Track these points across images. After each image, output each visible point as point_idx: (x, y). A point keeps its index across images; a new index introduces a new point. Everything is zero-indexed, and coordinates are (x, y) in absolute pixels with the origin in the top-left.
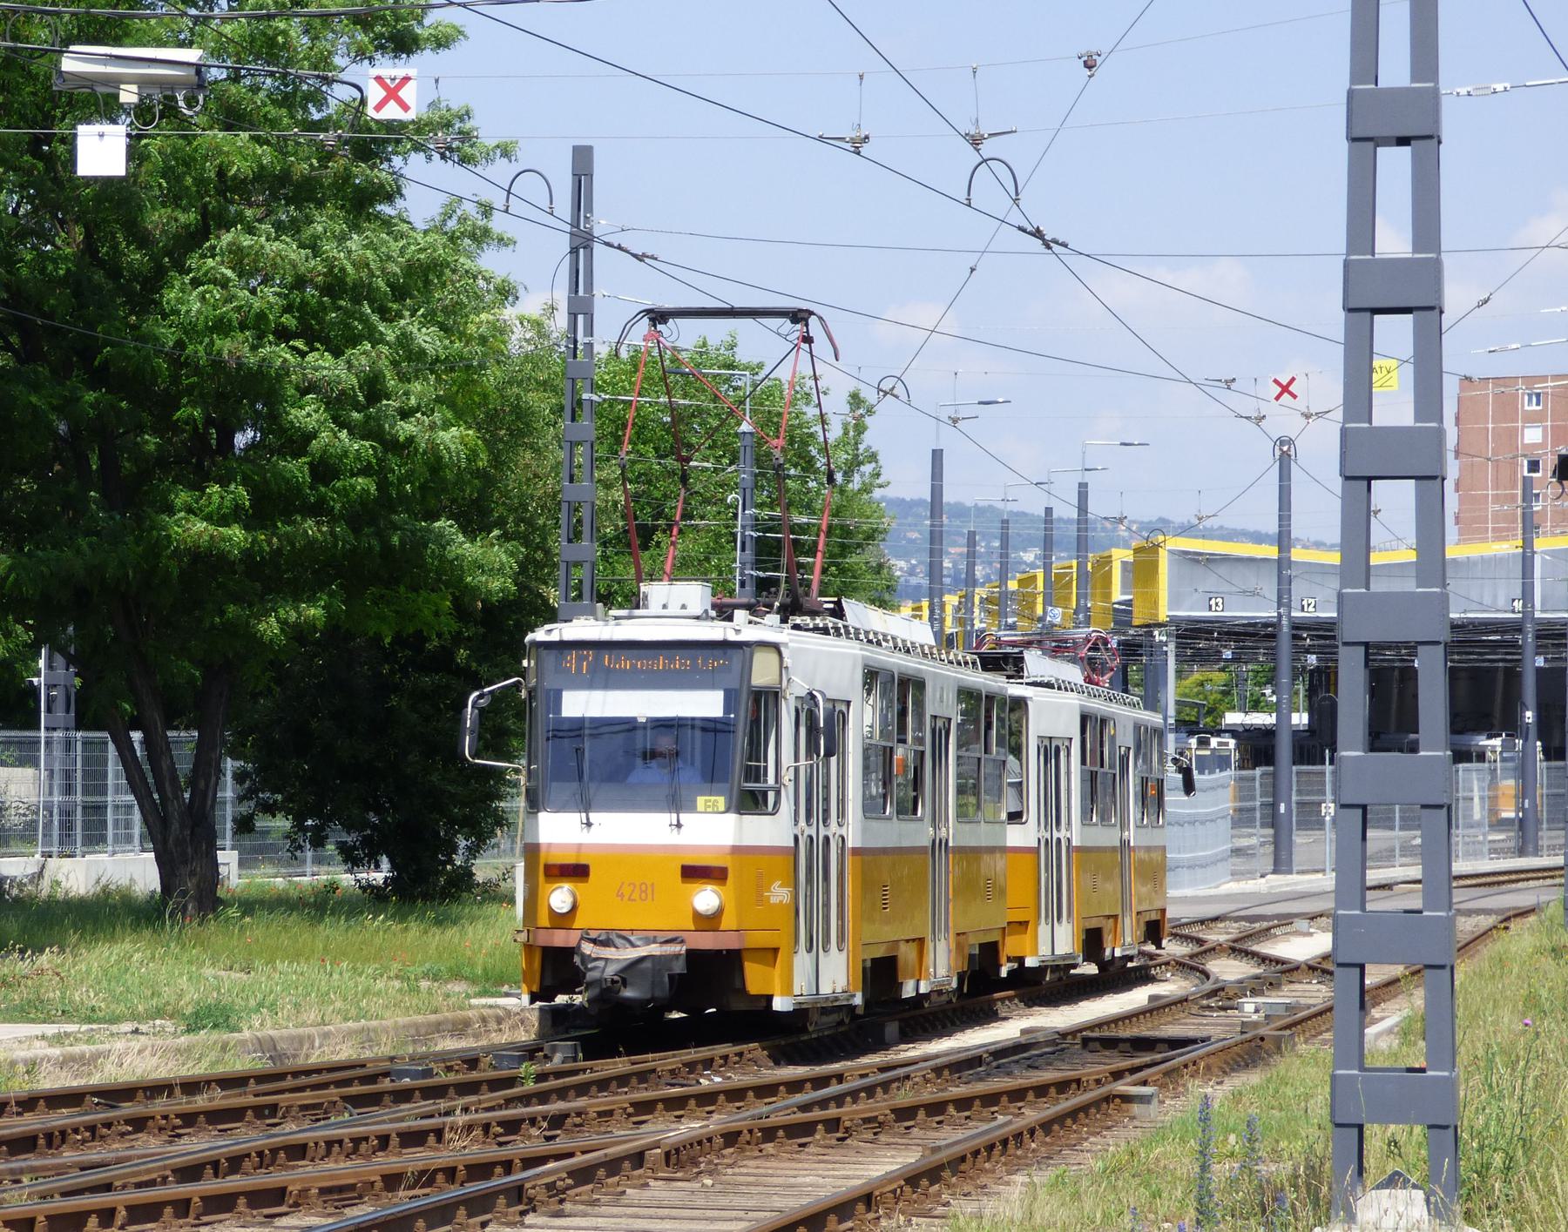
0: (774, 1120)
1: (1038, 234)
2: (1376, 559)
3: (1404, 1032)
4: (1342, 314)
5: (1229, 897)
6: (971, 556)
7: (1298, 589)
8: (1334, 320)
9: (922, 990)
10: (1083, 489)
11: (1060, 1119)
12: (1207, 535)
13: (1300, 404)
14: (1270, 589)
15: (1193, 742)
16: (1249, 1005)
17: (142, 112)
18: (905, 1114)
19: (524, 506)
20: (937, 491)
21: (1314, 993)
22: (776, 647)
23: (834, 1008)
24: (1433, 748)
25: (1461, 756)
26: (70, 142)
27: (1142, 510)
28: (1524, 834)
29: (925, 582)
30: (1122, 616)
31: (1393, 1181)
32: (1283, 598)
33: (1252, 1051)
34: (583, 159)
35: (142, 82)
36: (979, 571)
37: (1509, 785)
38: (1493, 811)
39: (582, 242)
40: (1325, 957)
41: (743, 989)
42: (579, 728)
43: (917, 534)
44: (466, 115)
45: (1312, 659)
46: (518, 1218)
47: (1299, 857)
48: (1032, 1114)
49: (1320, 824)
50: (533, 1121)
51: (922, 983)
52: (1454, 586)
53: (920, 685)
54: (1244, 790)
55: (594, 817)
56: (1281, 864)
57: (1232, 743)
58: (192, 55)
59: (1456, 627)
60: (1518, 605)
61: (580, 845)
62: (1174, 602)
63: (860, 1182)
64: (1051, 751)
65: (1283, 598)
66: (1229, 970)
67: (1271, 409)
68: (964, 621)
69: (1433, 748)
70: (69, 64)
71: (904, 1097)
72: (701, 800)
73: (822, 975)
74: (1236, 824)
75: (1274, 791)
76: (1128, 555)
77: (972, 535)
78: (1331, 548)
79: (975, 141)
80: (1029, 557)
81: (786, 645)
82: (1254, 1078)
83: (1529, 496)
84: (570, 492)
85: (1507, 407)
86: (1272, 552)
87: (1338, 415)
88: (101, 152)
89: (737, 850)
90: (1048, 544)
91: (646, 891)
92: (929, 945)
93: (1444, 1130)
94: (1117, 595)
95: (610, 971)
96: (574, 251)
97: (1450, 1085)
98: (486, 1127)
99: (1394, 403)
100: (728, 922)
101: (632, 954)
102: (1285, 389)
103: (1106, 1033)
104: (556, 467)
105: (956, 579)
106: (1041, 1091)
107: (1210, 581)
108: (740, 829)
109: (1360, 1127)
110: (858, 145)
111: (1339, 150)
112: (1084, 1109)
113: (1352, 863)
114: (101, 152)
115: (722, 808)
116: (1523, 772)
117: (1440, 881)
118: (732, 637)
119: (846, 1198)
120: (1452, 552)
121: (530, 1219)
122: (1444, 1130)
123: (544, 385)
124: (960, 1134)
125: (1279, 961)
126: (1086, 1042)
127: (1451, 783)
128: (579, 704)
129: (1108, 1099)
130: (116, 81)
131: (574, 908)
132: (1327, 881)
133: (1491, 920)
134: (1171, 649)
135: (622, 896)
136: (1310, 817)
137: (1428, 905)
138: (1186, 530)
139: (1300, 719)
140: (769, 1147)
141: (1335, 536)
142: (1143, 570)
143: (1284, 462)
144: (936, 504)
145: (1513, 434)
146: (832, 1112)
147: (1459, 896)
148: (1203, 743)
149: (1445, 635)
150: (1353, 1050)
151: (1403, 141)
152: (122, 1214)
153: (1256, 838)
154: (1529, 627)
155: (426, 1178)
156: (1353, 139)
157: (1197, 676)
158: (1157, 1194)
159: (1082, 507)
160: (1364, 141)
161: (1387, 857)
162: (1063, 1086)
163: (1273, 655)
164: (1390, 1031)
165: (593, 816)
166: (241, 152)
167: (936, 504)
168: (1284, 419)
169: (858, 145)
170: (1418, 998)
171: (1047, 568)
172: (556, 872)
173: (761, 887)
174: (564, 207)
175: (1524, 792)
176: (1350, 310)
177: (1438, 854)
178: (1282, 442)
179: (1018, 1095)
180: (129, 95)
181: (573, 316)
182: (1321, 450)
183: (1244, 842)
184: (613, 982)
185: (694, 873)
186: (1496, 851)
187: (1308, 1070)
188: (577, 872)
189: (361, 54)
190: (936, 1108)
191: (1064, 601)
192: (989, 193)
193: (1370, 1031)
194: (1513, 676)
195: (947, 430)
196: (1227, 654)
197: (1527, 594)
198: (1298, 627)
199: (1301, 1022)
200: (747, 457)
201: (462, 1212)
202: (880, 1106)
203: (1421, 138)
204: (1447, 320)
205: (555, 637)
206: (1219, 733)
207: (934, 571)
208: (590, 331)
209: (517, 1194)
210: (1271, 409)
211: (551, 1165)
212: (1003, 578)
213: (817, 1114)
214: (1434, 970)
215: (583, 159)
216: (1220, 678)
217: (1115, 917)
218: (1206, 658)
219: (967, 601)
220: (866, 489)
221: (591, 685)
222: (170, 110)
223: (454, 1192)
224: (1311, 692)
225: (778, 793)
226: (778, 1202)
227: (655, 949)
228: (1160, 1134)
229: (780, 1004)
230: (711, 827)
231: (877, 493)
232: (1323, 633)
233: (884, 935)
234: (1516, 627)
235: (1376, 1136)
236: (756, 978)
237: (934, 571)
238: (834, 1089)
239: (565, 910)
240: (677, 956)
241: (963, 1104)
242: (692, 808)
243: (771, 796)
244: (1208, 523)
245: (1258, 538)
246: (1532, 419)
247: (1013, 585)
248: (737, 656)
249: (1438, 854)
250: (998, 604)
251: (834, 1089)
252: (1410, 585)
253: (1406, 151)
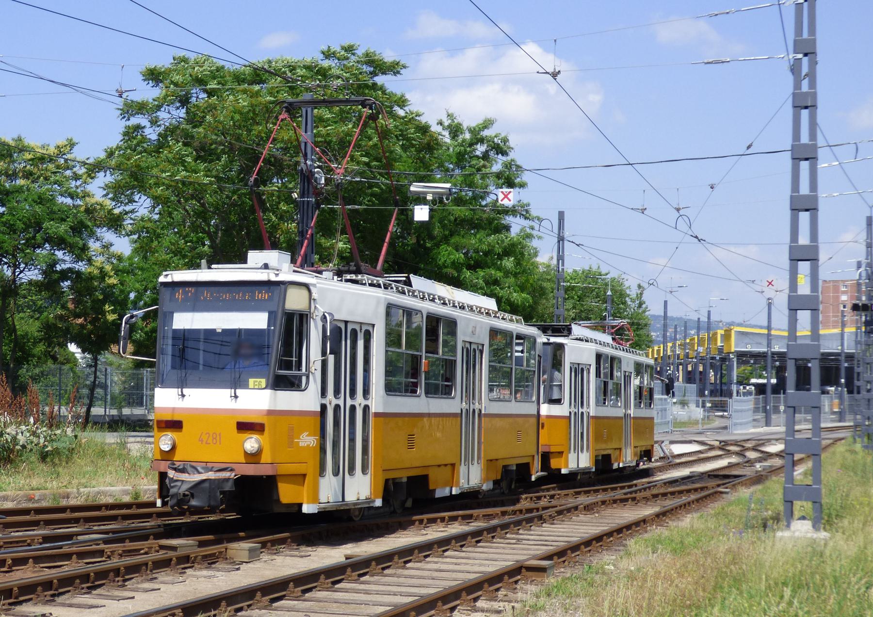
0: (616, 497)
1: (696, 237)
2: (798, 334)
3: (805, 474)
4: (788, 261)
5: (752, 434)
6: (676, 332)
7: (773, 342)
8: (786, 263)
9: (454, 493)
10: (709, 312)
11: (701, 498)
12: (746, 326)
13: (774, 288)
14: (765, 343)
15: (742, 387)
16: (758, 466)
17: (434, 202)
18: (655, 496)
19: (543, 316)
20: (665, 312)
21: (777, 462)
22: (306, 286)
23: (585, 472)
24: (815, 391)
25: (824, 392)
26: (412, 211)
27: (727, 319)
28: (841, 416)
29: (662, 340)
30: (720, 351)
31: (803, 518)
32: (769, 345)
33: (759, 479)
34: (561, 215)
35: (433, 193)
36: (678, 336)
37: (836, 401)
38: (831, 409)
39: (561, 239)
40: (781, 452)
41: (278, 500)
42: (185, 338)
43: (659, 325)
44: (529, 205)
45: (778, 363)
46: (380, 571)
47: (773, 422)
48: (693, 497)
49: (779, 412)
50: (545, 497)
51: (454, 489)
52: (821, 342)
53: (452, 325)
54: (757, 402)
55: (186, 391)
56: (768, 424)
57: (753, 388)
58: (448, 185)
59: (823, 354)
60: (840, 348)
61: (174, 409)
62: (736, 346)
63: (411, 599)
64: (578, 370)
65: (769, 345)
66: (752, 455)
67: (766, 289)
68: (673, 351)
69: (815, 391)
70: (412, 189)
71: (655, 491)
72: (251, 381)
73: (581, 460)
74: (754, 412)
75: (766, 402)
76: (723, 332)
77: (676, 326)
78: (784, 330)
79: (678, 210)
80: (693, 332)
81: (314, 285)
82: (759, 487)
83: (843, 316)
84: (557, 312)
85: (836, 289)
86: (765, 331)
87: (787, 291)
88: (421, 214)
89: (270, 413)
90: (699, 329)
91: (216, 438)
92: (624, 450)
93: (817, 503)
94: (719, 344)
95: (185, 487)
96: (559, 242)
97: (819, 490)
98: (531, 498)
99: (804, 287)
100: (266, 457)
101: (197, 478)
102: (770, 283)
103: (715, 473)
104: (553, 306)
105: (671, 338)
106: (696, 490)
107: (747, 340)
108: (274, 400)
109: (792, 502)
110: (643, 211)
111: (788, 213)
112: (709, 495)
113: (791, 424)
114: (421, 214)
115: (264, 386)
116: (841, 397)
117: (817, 430)
118: (273, 278)
119: (498, 573)
120: (822, 332)
121: (544, 525)
122: (817, 503)
123: (549, 280)
124: (671, 502)
125: (767, 453)
126: (709, 476)
127: (820, 399)
128: (183, 321)
129: (716, 493)
130: (426, 193)
131: (174, 448)
132: (783, 429)
133: (831, 441)
134: (735, 359)
135: (202, 441)
136: (776, 410)
137: (814, 437)
138: (739, 325)
139: (774, 381)
140: (615, 505)
141: (786, 327)
142: (727, 337)
143: (770, 305)
144: (665, 316)
145: (838, 297)
146: (634, 495)
147: (822, 433)
148: (744, 388)
149: (819, 357)
150: (790, 479)
151: (807, 210)
152: (425, 521)
153: (760, 416)
154: (843, 355)
155: (514, 513)
156: (792, 210)
157: (743, 368)
158: (730, 521)
159: (709, 318)
160: (795, 210)
161: (800, 422)
162: (702, 489)
163: (765, 361)
164: (800, 474)
165: (185, 391)
166: (461, 211)
167: (665, 316)
168: (770, 292)
169: (643, 211)
170: (810, 464)
171: (698, 335)
172: (164, 425)
173: (292, 435)
174: (556, 230)
175: (841, 403)
176: (791, 260)
177: (816, 421)
178: (769, 299)
179: (689, 491)
180: (429, 197)
181: (558, 261)
182: (781, 301)
183: (756, 417)
184: (184, 495)
185: (244, 427)
186: (833, 421)
187: (776, 487)
188: (175, 425)
189: (499, 187)
190: (664, 495)
191: (703, 345)
192: (682, 225)
193: (795, 473)
194: (838, 369)
195: (669, 295)
196: (752, 361)
197: (842, 345)
198: (773, 354)
199: (774, 471)
200: (609, 302)
201: (349, 570)
202: (648, 494)
203: (812, 209)
204: (820, 263)
205: (169, 279)
206: (749, 385)
207: (665, 336)
208: (563, 265)
209: (540, 518)
210: (766, 289)
211: (551, 510)
212: (685, 339)
213: (629, 496)
214: (815, 456)
215: (561, 215)
216: (750, 368)
217: (453, 465)
218: (746, 363)
219: (674, 346)
220: (644, 312)
221: (194, 309)
222: (441, 201)
223: (522, 517)
224: (777, 373)
225: (308, 377)
226: (617, 521)
227: (211, 475)
228: (730, 504)
229: (564, 471)
230: (256, 398)
231: (647, 313)
232: (781, 356)
233: (607, 448)
234: (838, 354)
235: (797, 504)
236: (287, 494)
237: (665, 336)
238: (634, 489)
239: (167, 449)
240: (227, 480)
241: (672, 493)
242: (246, 386)
243: (304, 379)
244: (748, 323)
245: (761, 327)
246: (844, 293)
247: (688, 341)
248: (277, 290)
249: (816, 421)
250: (683, 346)
251: (634, 489)
252: (808, 342)
253: (808, 213)
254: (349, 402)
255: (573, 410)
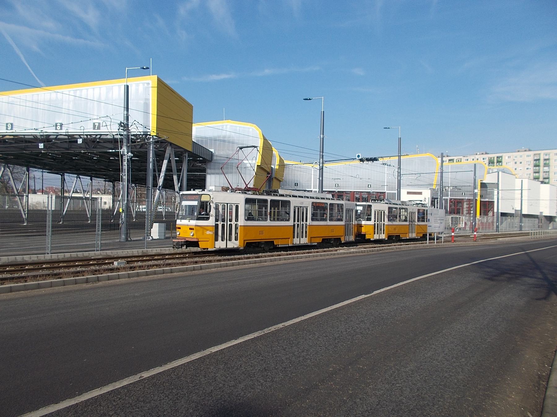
236: (367, 237)
254: (302, 223)
255: (376, 223)
